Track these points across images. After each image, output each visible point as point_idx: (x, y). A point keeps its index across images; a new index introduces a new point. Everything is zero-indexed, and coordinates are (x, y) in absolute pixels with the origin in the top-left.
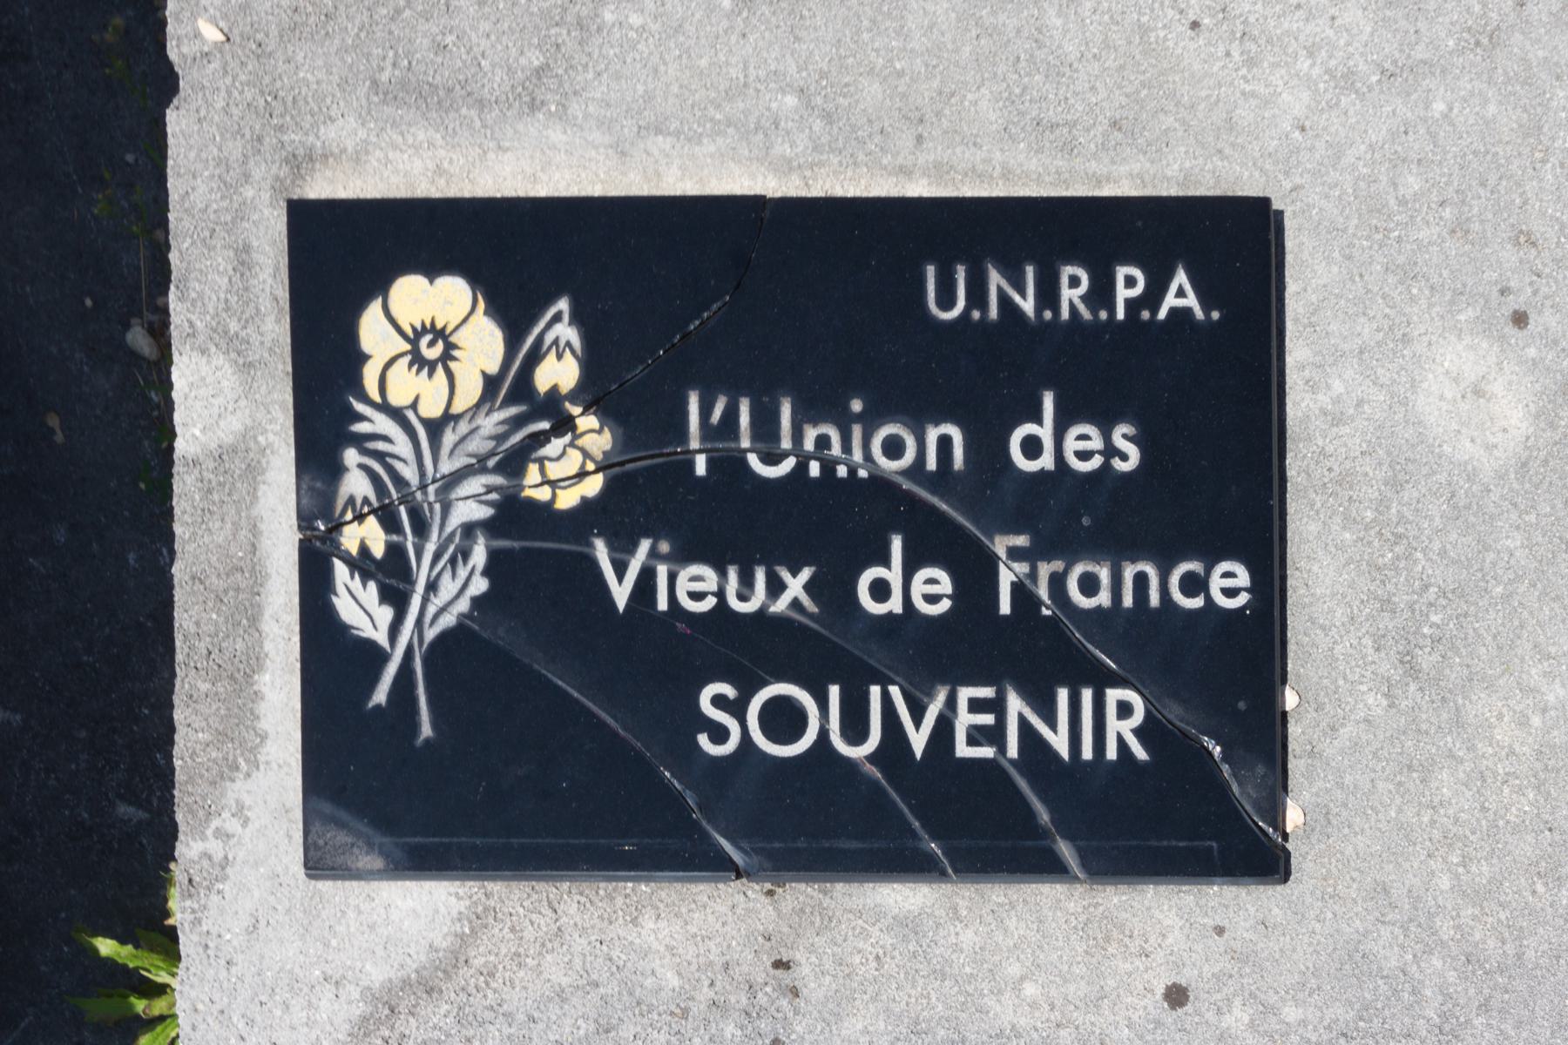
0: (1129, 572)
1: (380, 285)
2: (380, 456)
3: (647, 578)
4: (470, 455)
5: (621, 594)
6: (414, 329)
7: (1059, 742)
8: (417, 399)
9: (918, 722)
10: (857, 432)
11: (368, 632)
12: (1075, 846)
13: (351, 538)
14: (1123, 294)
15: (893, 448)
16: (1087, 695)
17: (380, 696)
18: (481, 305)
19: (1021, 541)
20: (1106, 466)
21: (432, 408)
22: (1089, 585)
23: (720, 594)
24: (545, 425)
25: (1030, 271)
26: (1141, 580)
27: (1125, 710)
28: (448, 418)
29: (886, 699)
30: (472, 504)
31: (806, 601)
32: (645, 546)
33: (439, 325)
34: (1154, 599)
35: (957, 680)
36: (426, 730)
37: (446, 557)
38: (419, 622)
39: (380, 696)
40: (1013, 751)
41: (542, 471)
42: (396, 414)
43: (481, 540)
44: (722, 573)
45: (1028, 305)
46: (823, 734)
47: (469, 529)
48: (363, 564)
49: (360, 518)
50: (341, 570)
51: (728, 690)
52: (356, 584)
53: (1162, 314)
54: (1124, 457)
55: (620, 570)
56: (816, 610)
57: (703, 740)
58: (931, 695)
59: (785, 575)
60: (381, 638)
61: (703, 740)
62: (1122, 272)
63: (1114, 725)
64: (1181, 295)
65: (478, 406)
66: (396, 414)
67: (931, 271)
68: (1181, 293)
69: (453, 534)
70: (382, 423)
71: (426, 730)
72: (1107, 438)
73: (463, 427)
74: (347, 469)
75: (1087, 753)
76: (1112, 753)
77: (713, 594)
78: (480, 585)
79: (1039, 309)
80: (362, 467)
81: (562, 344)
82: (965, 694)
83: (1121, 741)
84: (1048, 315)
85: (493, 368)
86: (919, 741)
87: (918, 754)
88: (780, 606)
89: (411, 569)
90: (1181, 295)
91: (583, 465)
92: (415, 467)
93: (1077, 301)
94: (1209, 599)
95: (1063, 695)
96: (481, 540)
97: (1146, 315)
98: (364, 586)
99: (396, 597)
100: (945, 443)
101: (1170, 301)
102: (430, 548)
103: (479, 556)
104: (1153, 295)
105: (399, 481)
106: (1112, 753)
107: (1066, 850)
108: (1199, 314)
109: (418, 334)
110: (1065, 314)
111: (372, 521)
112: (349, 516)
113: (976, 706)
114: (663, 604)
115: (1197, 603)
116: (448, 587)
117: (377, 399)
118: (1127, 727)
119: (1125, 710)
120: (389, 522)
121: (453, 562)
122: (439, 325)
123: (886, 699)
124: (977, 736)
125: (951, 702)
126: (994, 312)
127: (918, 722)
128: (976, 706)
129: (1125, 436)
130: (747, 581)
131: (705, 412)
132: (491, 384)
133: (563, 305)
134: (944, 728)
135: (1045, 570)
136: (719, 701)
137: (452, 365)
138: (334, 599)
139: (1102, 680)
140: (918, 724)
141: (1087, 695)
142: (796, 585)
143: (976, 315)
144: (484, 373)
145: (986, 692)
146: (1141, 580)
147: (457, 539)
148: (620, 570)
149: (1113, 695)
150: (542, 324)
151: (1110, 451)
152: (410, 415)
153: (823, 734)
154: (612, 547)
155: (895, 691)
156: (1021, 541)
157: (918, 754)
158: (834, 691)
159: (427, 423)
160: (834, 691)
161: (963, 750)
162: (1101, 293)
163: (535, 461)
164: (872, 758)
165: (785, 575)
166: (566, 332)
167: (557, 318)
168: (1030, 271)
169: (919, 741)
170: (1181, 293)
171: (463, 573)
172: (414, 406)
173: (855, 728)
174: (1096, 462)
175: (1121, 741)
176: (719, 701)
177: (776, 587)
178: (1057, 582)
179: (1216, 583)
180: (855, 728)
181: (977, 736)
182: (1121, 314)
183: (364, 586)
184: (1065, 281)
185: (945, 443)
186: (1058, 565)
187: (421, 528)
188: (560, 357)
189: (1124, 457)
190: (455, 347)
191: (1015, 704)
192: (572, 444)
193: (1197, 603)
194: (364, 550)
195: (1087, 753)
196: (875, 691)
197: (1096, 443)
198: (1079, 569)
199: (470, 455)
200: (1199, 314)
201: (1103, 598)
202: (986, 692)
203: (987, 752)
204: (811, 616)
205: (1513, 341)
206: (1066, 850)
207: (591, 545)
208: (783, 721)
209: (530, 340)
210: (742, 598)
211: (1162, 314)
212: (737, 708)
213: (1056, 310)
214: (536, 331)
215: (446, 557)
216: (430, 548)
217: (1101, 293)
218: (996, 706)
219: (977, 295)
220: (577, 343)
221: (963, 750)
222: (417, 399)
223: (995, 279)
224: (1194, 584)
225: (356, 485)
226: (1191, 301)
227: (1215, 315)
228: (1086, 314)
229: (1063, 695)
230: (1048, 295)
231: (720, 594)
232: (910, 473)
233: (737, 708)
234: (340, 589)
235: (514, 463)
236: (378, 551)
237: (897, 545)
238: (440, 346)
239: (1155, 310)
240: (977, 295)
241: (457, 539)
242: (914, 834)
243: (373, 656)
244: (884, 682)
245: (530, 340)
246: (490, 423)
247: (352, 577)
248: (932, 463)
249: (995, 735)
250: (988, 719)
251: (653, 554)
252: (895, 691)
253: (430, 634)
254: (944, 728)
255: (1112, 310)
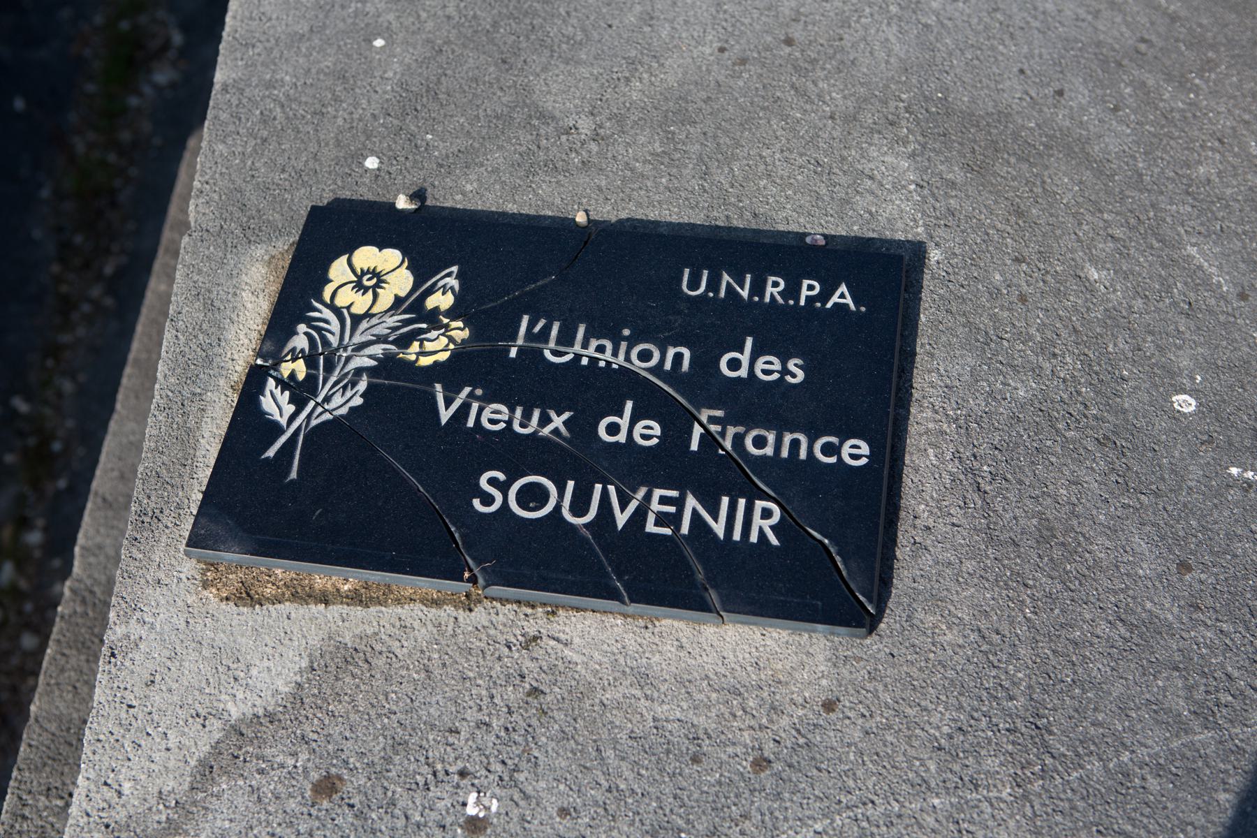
0: (788, 438)
1: (350, 249)
2: (319, 330)
3: (464, 409)
4: (373, 335)
5: (445, 415)
6: (362, 270)
7: (719, 529)
8: (352, 304)
9: (623, 508)
10: (624, 345)
11: (277, 417)
12: (718, 592)
13: (286, 369)
14: (805, 293)
15: (646, 356)
16: (742, 502)
17: (271, 453)
18: (406, 264)
19: (719, 413)
20: (781, 380)
21: (359, 309)
22: (760, 442)
23: (509, 423)
24: (424, 326)
25: (748, 277)
26: (795, 444)
27: (767, 514)
28: (368, 315)
29: (605, 493)
30: (366, 359)
31: (563, 429)
32: (467, 390)
33: (378, 270)
34: (803, 454)
35: (653, 484)
36: (294, 475)
37: (341, 384)
38: (309, 417)
39: (271, 453)
40: (685, 529)
41: (421, 346)
42: (337, 311)
43: (365, 377)
44: (512, 410)
45: (745, 294)
46: (558, 508)
47: (359, 372)
48: (287, 384)
49: (294, 360)
50: (271, 383)
51: (501, 476)
52: (278, 392)
53: (829, 305)
54: (794, 376)
55: (448, 403)
56: (568, 435)
57: (476, 503)
58: (635, 491)
59: (553, 414)
60: (284, 422)
61: (476, 503)
62: (806, 283)
63: (757, 521)
64: (842, 296)
65: (386, 312)
66: (337, 311)
67: (687, 271)
68: (842, 296)
69: (348, 373)
70: (327, 314)
71: (294, 475)
72: (784, 364)
73: (374, 321)
74: (298, 334)
75: (737, 536)
76: (754, 538)
77: (505, 422)
78: (358, 401)
79: (751, 295)
80: (306, 333)
81: (448, 286)
82: (658, 493)
83: (761, 531)
84: (756, 299)
85: (403, 294)
86: (621, 519)
87: (620, 526)
88: (546, 431)
89: (317, 388)
90: (842, 296)
91: (447, 345)
92: (338, 337)
93: (776, 294)
94: (840, 459)
95: (725, 501)
96: (365, 377)
97: (819, 305)
98: (282, 393)
99: (299, 402)
100: (678, 358)
101: (835, 299)
102: (333, 379)
103: (362, 386)
104: (825, 295)
105: (326, 343)
106: (754, 538)
107: (713, 596)
108: (852, 307)
109: (363, 273)
110: (767, 299)
111: (301, 361)
112: (289, 357)
113: (664, 500)
114: (471, 423)
115: (833, 460)
116: (337, 400)
117: (328, 300)
118: (767, 524)
119: (767, 514)
120: (311, 362)
121: (345, 388)
122: (378, 270)
123: (605, 493)
124: (661, 520)
125: (648, 497)
126: (722, 294)
127: (623, 508)
128: (664, 500)
129: (796, 365)
130: (527, 416)
131: (531, 325)
132: (398, 301)
133: (455, 269)
134: (641, 513)
135: (731, 431)
136: (492, 482)
137: (379, 290)
138: (261, 398)
139: (753, 494)
140: (622, 510)
141: (742, 502)
142: (558, 421)
143: (711, 295)
144: (396, 296)
145: (674, 493)
146: (795, 444)
147: (350, 376)
148: (448, 403)
149: (760, 504)
150: (438, 277)
151: (785, 371)
152: (345, 311)
153: (558, 508)
154: (445, 388)
155: (611, 488)
156: (719, 413)
157: (620, 526)
158: (571, 484)
159: (353, 316)
160: (571, 484)
161: (650, 527)
162: (792, 291)
163: (417, 340)
164: (586, 526)
165: (553, 414)
166: (453, 282)
167: (449, 275)
168: (748, 277)
169: (621, 519)
170: (842, 296)
171: (349, 394)
172: (348, 308)
173: (580, 506)
174: (776, 376)
175: (761, 531)
176: (492, 482)
177: (545, 420)
178: (739, 440)
179: (846, 451)
180: (580, 506)
181: (661, 520)
182: (802, 303)
183: (282, 393)
184: (770, 283)
185: (678, 358)
186: (741, 429)
187: (329, 368)
188: (444, 293)
189: (794, 376)
190: (384, 282)
191: (691, 502)
192: (443, 334)
193: (833, 460)
194: (292, 375)
195: (737, 536)
196: (598, 487)
197: (777, 366)
198: (754, 433)
199: (373, 335)
200: (852, 307)
201: (769, 451)
202: (674, 493)
203: (667, 531)
204: (564, 439)
205: (223, 197)
206: (713, 596)
207: (434, 387)
208: (532, 496)
209: (429, 283)
210: (523, 425)
211: (829, 305)
212: (504, 488)
213: (762, 296)
214: (434, 280)
215: (341, 384)
216: (333, 379)
217: (792, 291)
218: (679, 503)
219: (714, 284)
220: (457, 288)
221: (650, 527)
222: (352, 304)
223: (726, 278)
224: (828, 450)
225: (300, 341)
226: (849, 300)
227: (863, 309)
228: (780, 300)
229: (725, 501)
230: (758, 288)
231: (509, 423)
232: (654, 371)
233: (504, 488)
234: (268, 393)
235: (404, 342)
236: (301, 376)
237: (629, 405)
238: (375, 280)
239: (824, 303)
240: (714, 284)
241: (350, 376)
242: (607, 575)
243: (277, 430)
244: (605, 483)
245: (429, 283)
246: (392, 321)
247: (276, 388)
248: (668, 366)
249: (674, 520)
250: (672, 509)
251: (471, 395)
252: (611, 488)
253: (314, 423)
254: (641, 513)
255: (797, 299)
